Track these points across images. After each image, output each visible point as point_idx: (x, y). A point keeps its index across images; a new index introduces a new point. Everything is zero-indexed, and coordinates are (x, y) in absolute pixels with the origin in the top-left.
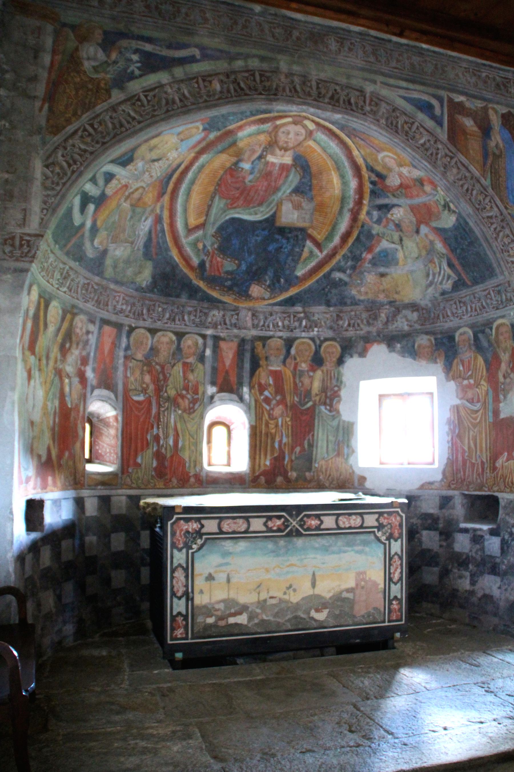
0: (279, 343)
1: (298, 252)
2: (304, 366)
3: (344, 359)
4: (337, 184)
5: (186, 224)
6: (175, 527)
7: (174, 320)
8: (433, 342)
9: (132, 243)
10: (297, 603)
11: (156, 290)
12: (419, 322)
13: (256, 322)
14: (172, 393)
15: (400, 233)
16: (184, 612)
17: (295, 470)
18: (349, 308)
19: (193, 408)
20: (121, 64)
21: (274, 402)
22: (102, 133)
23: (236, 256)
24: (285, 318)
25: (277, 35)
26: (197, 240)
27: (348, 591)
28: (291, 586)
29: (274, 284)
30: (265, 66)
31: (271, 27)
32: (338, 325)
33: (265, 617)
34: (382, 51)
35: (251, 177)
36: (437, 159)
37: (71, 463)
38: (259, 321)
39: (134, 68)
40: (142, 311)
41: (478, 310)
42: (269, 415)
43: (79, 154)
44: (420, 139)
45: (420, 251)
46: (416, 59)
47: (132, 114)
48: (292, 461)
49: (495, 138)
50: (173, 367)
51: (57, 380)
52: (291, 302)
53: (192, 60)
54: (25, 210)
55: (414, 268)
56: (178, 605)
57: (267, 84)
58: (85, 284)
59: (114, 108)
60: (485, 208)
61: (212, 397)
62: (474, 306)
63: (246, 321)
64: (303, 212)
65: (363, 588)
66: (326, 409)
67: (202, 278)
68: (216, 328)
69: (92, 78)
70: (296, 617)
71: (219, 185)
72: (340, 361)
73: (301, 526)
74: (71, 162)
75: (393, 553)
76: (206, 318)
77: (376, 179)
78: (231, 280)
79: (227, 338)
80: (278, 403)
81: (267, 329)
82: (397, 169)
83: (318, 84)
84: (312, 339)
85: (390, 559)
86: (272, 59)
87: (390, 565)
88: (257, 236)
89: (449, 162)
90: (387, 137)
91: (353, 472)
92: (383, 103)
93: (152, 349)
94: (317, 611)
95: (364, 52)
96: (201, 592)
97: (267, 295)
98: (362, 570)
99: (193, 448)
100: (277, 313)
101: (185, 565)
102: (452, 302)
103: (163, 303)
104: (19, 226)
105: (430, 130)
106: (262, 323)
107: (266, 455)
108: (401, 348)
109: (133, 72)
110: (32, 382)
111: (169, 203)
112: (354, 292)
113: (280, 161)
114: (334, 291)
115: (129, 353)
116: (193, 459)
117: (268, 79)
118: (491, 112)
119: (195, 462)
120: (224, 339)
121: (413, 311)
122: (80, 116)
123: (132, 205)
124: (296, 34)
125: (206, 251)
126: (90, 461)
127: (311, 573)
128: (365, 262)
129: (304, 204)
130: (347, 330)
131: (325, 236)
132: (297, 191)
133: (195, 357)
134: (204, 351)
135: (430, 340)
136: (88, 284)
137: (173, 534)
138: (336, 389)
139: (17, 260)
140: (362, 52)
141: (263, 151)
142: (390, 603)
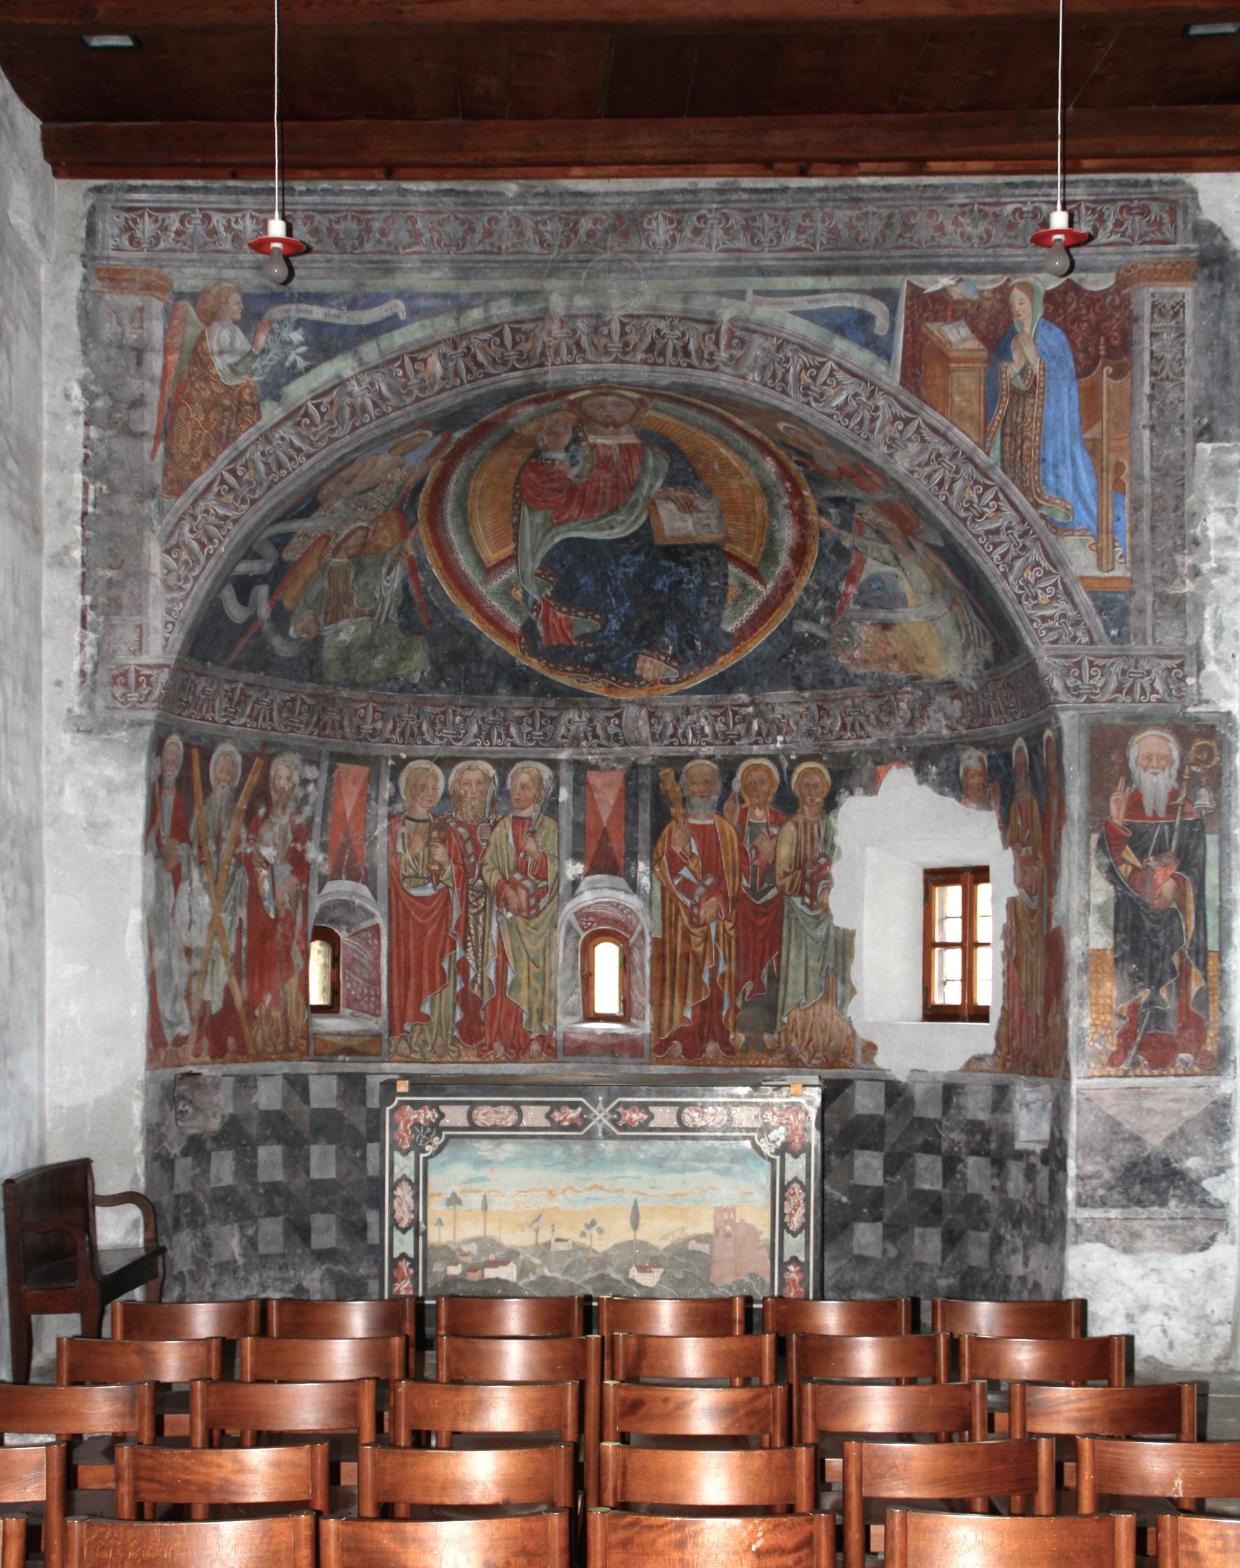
0: (707, 770)
2: (759, 816)
5: (479, 562)
6: (397, 1115)
7: (489, 737)
9: (372, 614)
10: (605, 1253)
13: (658, 729)
14: (493, 878)
16: (411, 1254)
17: (743, 1030)
18: (839, 693)
19: (536, 906)
20: (274, 354)
21: (701, 890)
22: (249, 483)
23: (590, 607)
24: (716, 717)
25: (548, 236)
26: (508, 586)
27: (699, 1239)
28: (593, 1224)
29: (682, 651)
30: (523, 310)
31: (536, 223)
33: (547, 1272)
34: (766, 218)
35: (576, 470)
36: (872, 431)
37: (276, 1014)
38: (665, 727)
39: (296, 357)
40: (420, 727)
42: (691, 916)
43: (217, 526)
44: (837, 394)
46: (843, 216)
47: (297, 442)
48: (737, 1010)
49: (1023, 354)
50: (493, 828)
51: (242, 877)
52: (724, 684)
53: (392, 323)
54: (140, 627)
56: (401, 1241)
57: (526, 347)
58: (286, 702)
59: (266, 437)
60: (981, 516)
61: (575, 884)
65: (728, 1235)
66: (803, 903)
67: (534, 653)
68: (578, 745)
69: (230, 387)
70: (602, 1277)
72: (831, 804)
73: (614, 1122)
74: (205, 540)
75: (788, 1177)
78: (594, 650)
79: (602, 765)
80: (710, 892)
83: (623, 325)
84: (773, 758)
85: (784, 1188)
86: (535, 294)
87: (783, 1199)
88: (625, 566)
89: (901, 432)
91: (854, 1033)
92: (756, 336)
93: (446, 795)
94: (642, 1269)
95: (727, 231)
96: (440, 1222)
97: (673, 674)
98: (726, 1204)
99: (535, 984)
100: (699, 708)
101: (413, 1178)
104: (134, 653)
105: (860, 372)
106: (670, 731)
107: (684, 997)
108: (939, 774)
109: (294, 364)
110: (184, 887)
112: (842, 660)
114: (804, 659)
115: (399, 807)
116: (535, 1006)
117: (528, 335)
118: (1017, 296)
119: (541, 1012)
120: (595, 768)
121: (953, 698)
122: (214, 459)
123: (350, 557)
124: (586, 224)
126: (331, 1009)
127: (631, 1203)
128: (847, 601)
129: (696, 503)
130: (840, 738)
132: (671, 481)
133: (538, 806)
134: (556, 793)
135: (981, 759)
136: (293, 700)
137: (394, 1126)
138: (823, 861)
139: (133, 708)
140: (721, 232)
142: (783, 1267)
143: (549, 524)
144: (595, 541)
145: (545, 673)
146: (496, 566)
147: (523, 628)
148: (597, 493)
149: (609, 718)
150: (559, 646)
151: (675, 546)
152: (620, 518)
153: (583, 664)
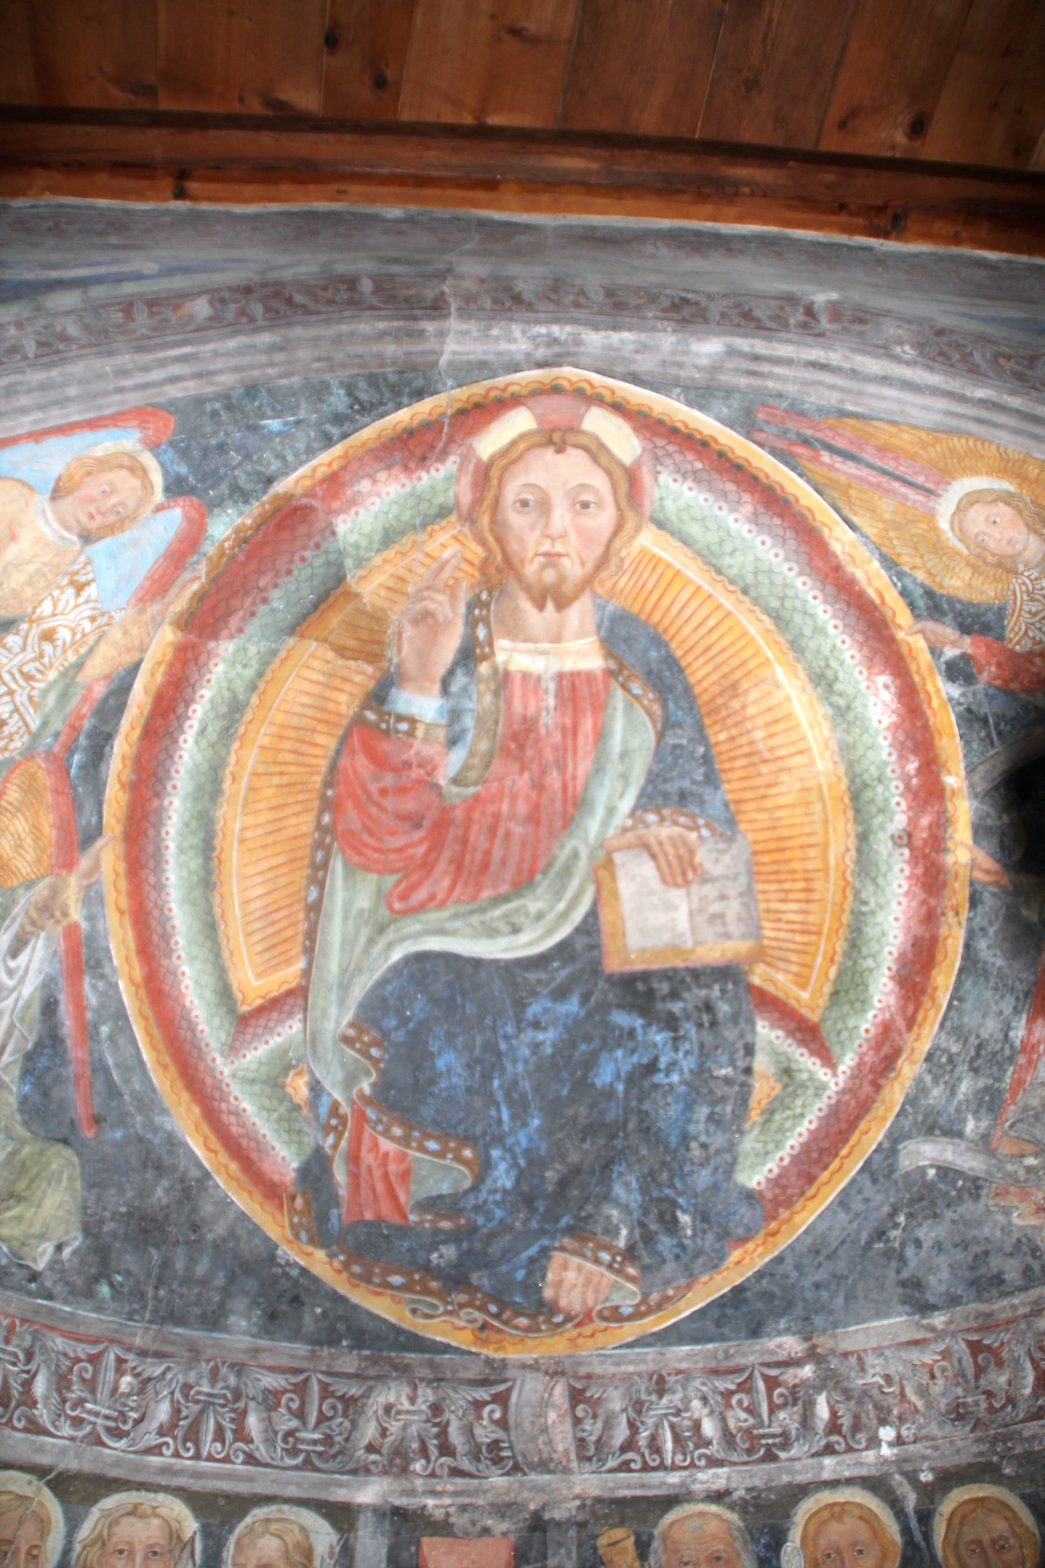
1: (728, 1081)
5: (225, 994)
7: (193, 1434)
11: (105, 1290)
13: (592, 1429)
29: (649, 1239)
32: (989, 1394)
38: (608, 1425)
40: (28, 1384)
63: (544, 1430)
64: (709, 890)
68: (404, 1471)
71: (328, 805)
76: (354, 1424)
77: (967, 645)
78: (454, 1237)
79: (460, 1521)
81: (653, 1461)
84: (876, 1484)
88: (536, 1025)
90: (934, 391)
97: (628, 1296)
103: (143, 1353)
106: (621, 1433)
111: (123, 884)
114: (927, 1233)
125: (324, 1110)
129: (703, 857)
131: (827, 989)
141: (472, 623)
143: (384, 913)
144: (477, 963)
145: (342, 1286)
146: (260, 1011)
147: (304, 1173)
148: (493, 831)
149: (478, 1405)
150: (378, 1222)
151: (646, 976)
152: (534, 906)
153: (427, 1269)
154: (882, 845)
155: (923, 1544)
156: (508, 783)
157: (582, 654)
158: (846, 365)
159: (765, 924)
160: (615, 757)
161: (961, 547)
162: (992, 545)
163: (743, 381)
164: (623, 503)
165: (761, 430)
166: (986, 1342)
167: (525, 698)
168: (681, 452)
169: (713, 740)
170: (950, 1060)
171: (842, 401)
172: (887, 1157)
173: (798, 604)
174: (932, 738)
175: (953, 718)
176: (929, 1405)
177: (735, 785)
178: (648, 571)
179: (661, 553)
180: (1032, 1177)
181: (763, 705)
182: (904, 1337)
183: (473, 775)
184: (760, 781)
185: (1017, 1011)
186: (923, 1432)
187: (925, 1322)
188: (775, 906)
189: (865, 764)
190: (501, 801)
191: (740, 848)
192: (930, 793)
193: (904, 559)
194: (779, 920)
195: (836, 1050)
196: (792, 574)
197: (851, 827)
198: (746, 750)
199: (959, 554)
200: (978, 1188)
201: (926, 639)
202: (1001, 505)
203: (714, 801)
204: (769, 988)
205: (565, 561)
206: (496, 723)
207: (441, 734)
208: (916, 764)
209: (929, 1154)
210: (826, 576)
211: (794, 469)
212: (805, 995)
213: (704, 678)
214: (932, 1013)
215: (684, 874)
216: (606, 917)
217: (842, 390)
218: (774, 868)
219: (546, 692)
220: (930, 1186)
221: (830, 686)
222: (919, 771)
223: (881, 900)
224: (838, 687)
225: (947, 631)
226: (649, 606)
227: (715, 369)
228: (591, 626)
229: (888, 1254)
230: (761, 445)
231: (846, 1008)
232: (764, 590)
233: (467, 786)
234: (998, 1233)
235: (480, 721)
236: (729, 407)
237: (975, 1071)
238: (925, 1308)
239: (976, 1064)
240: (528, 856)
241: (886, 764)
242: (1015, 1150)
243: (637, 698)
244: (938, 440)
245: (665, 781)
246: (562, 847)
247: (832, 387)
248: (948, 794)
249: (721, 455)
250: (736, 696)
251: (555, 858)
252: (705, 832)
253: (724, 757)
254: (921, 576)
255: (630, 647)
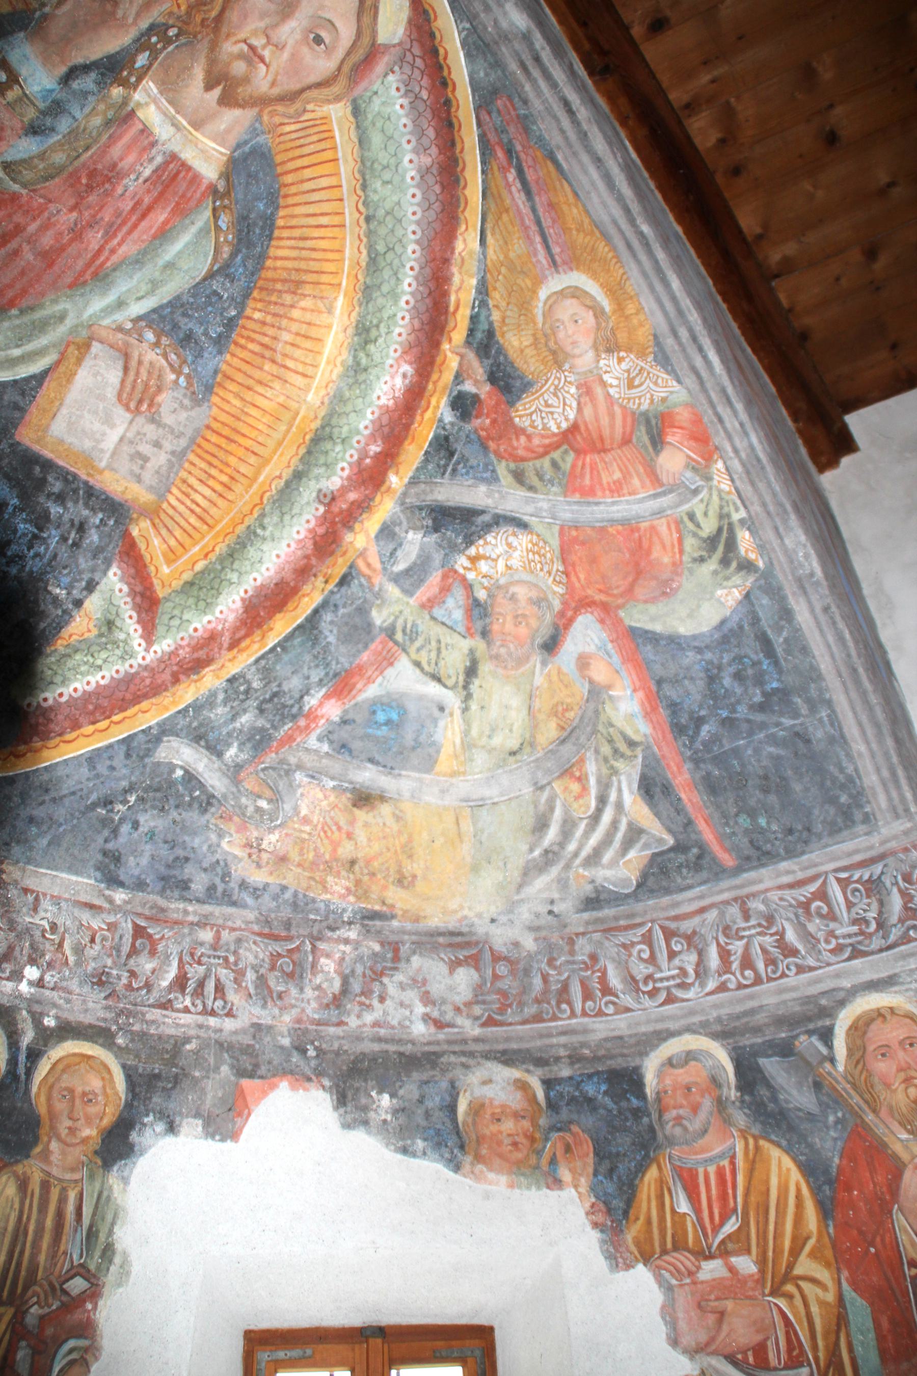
3: (134, 1136)
4: (330, 362)
8: (540, 1094)
12: (477, 1010)
15: (479, 644)
32: (133, 974)
41: (760, 965)
45: (534, 725)
55: (491, 792)
62: (737, 947)
64: (151, 430)
82: (585, 359)
102: (636, 935)
108: (396, 1112)
113: (175, 147)
114: (148, 820)
129: (166, 399)
130: (166, 1005)
131: (187, 576)
135: (522, 1086)
138: (77, 1285)
141: (141, 43)
151: (48, 465)
154: (308, 492)
155: (23, 1077)
156: (53, 208)
157: (204, 153)
158: (585, 126)
159: (175, 491)
160: (161, 262)
161: (540, 319)
162: (561, 335)
163: (513, 66)
164: (346, 69)
165: (489, 113)
166: (150, 931)
167: (129, 148)
168: (422, 73)
169: (248, 312)
170: (247, 692)
171: (559, 148)
172: (149, 741)
173: (396, 262)
174: (405, 438)
175: (431, 435)
176: (78, 963)
177: (236, 362)
178: (315, 138)
179: (337, 134)
180: (258, 817)
181: (308, 317)
182: (84, 898)
183: (28, 175)
184: (257, 374)
185: (321, 683)
186: (64, 984)
187: (107, 892)
188: (192, 481)
189: (344, 420)
190: (34, 219)
191: (200, 415)
192: (371, 478)
193: (496, 295)
194: (188, 496)
195: (161, 630)
196: (412, 237)
197: (295, 461)
198: (266, 340)
199: (535, 323)
200: (209, 804)
201: (460, 364)
202: (591, 313)
203: (211, 361)
204: (142, 546)
205: (262, 68)
206: (88, 148)
207: (31, 114)
208: (378, 449)
209: (185, 757)
210: (434, 260)
211: (483, 163)
212: (165, 570)
213: (282, 258)
214: (256, 646)
215: (140, 402)
216: (49, 386)
217: (566, 139)
218: (214, 450)
219: (151, 160)
220: (172, 783)
221: (366, 343)
222: (377, 456)
223: (277, 534)
224: (371, 348)
225: (479, 370)
226: (291, 166)
227: (506, 37)
228: (232, 140)
229: (105, 822)
230: (479, 124)
231: (191, 601)
232: (382, 231)
233: (14, 180)
234: (205, 848)
235: (73, 134)
236: (487, 75)
237: (261, 711)
238: (113, 881)
239: (265, 706)
240: (18, 286)
241: (358, 432)
242: (256, 789)
243: (218, 228)
244: (592, 233)
245: (185, 315)
246: (55, 301)
247: (562, 131)
248: (383, 489)
249: (448, 103)
250: (294, 293)
251: (41, 306)
252: (182, 380)
253: (245, 333)
254: (496, 316)
255: (248, 184)
